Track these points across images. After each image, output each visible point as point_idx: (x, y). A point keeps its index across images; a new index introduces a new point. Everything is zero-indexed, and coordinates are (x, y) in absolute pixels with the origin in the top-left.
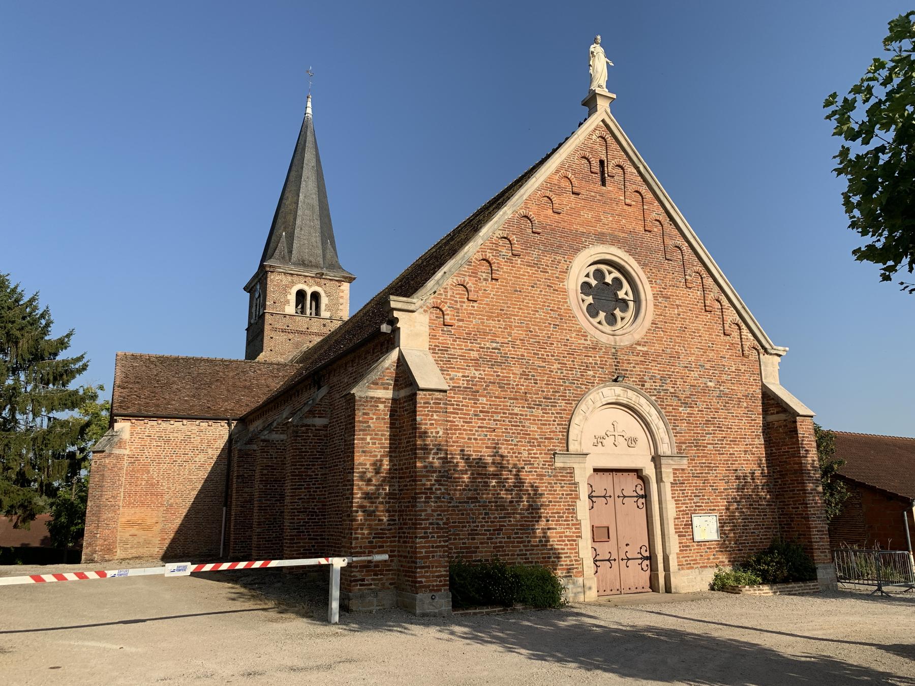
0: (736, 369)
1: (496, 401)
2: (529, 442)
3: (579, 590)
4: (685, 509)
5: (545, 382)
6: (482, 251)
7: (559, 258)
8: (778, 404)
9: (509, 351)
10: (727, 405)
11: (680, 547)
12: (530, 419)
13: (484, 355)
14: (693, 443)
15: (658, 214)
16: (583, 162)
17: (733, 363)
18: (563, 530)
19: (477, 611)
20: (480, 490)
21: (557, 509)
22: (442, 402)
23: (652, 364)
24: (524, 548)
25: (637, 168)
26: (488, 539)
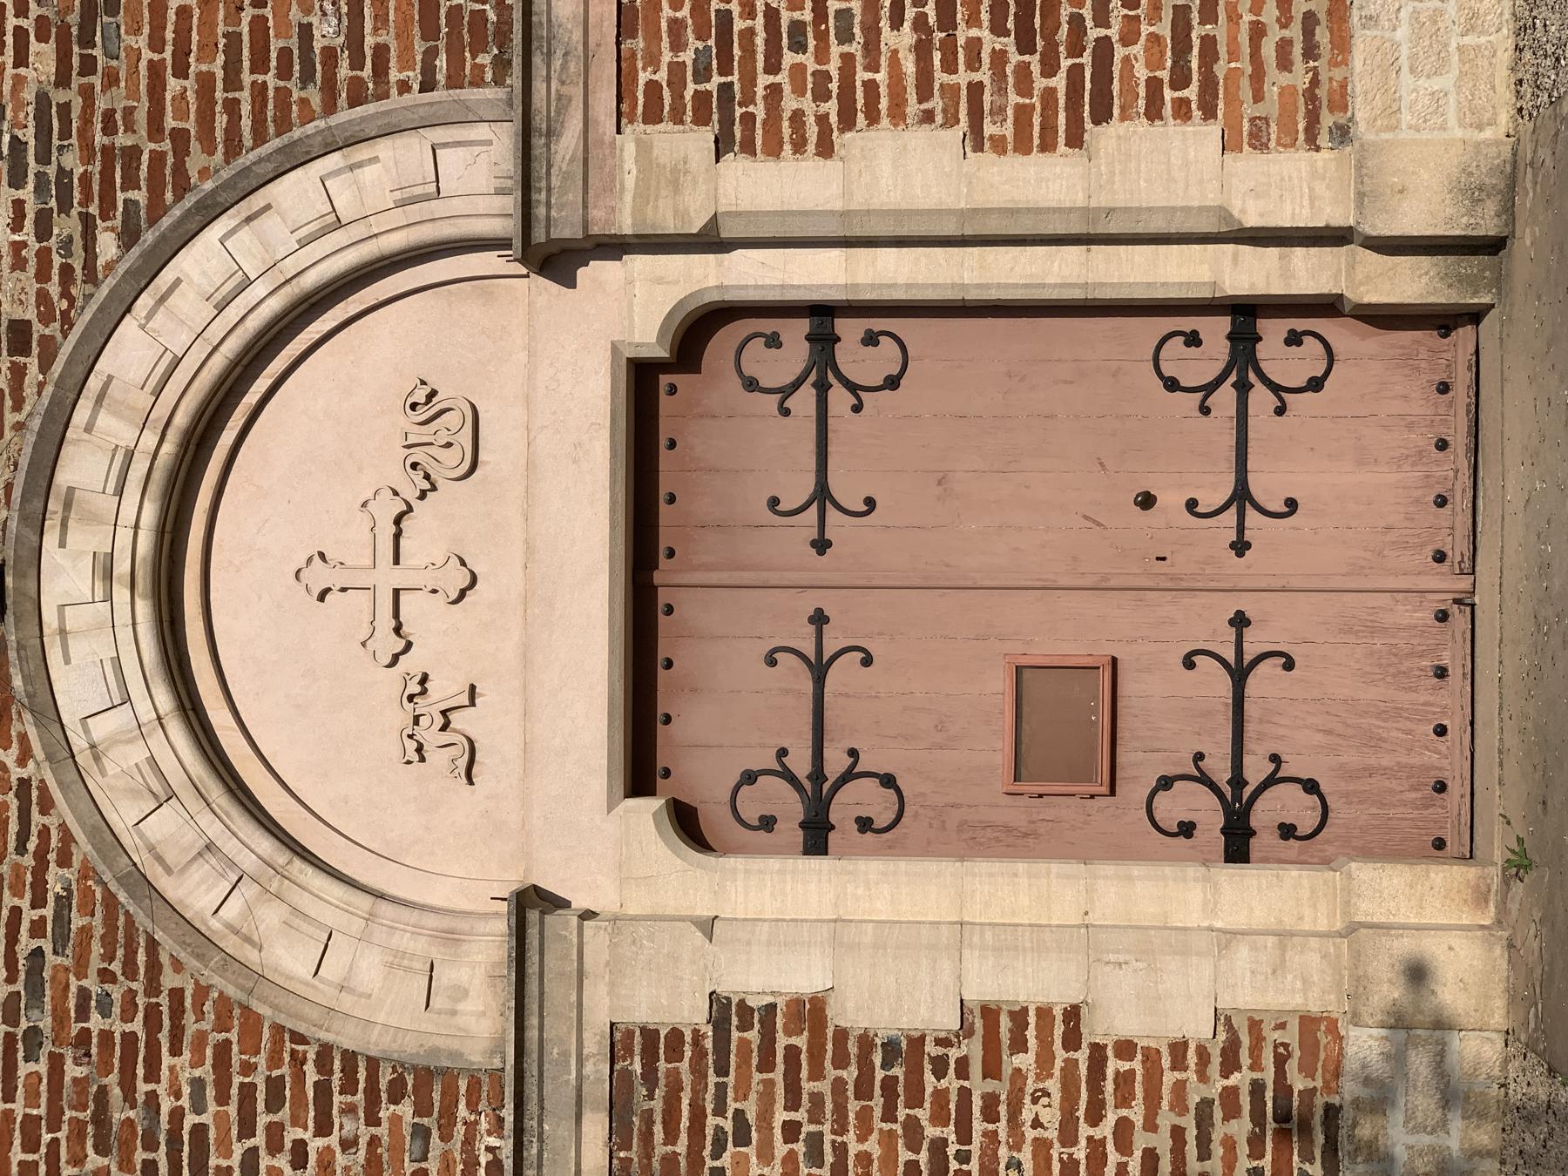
3: (1420, 1063)
11: (1182, 110)
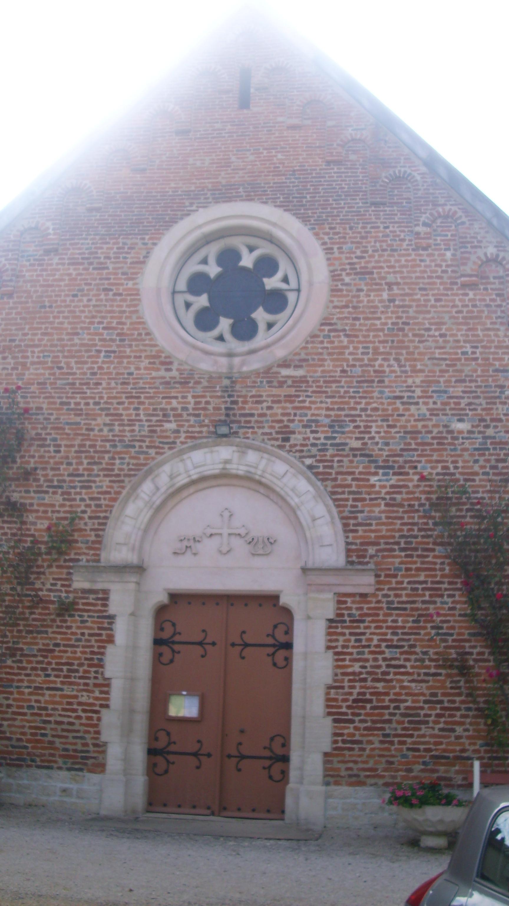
5: (76, 448)
14: (398, 543)
18: (75, 693)
21: (68, 658)
23: (313, 399)
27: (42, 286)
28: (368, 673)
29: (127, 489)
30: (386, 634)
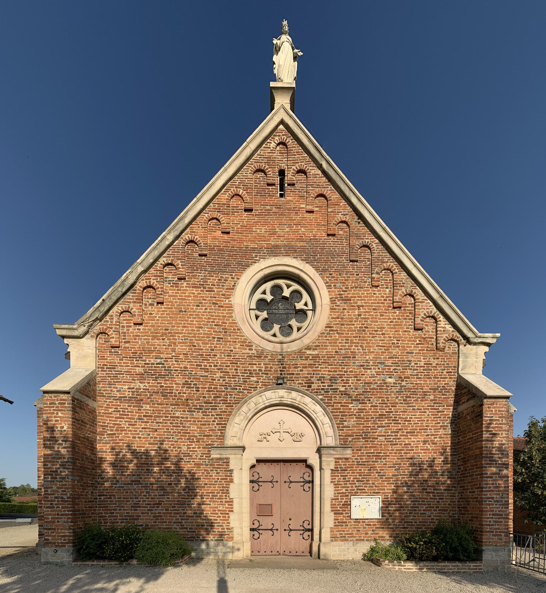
0: (425, 364)
1: (158, 407)
2: (188, 439)
3: (229, 550)
4: (344, 491)
5: (207, 389)
6: (146, 279)
7: (227, 276)
8: (469, 390)
9: (173, 364)
10: (408, 399)
12: (190, 421)
13: (149, 370)
14: (362, 436)
15: (344, 215)
16: (259, 176)
17: (422, 357)
18: (216, 506)
19: (95, 563)
20: (142, 475)
21: (212, 490)
22: (66, 402)
23: (322, 366)
24: (180, 518)
25: (320, 167)
26: (148, 510)
27: (179, 299)
28: (348, 493)
29: (235, 410)
30: (357, 476)
